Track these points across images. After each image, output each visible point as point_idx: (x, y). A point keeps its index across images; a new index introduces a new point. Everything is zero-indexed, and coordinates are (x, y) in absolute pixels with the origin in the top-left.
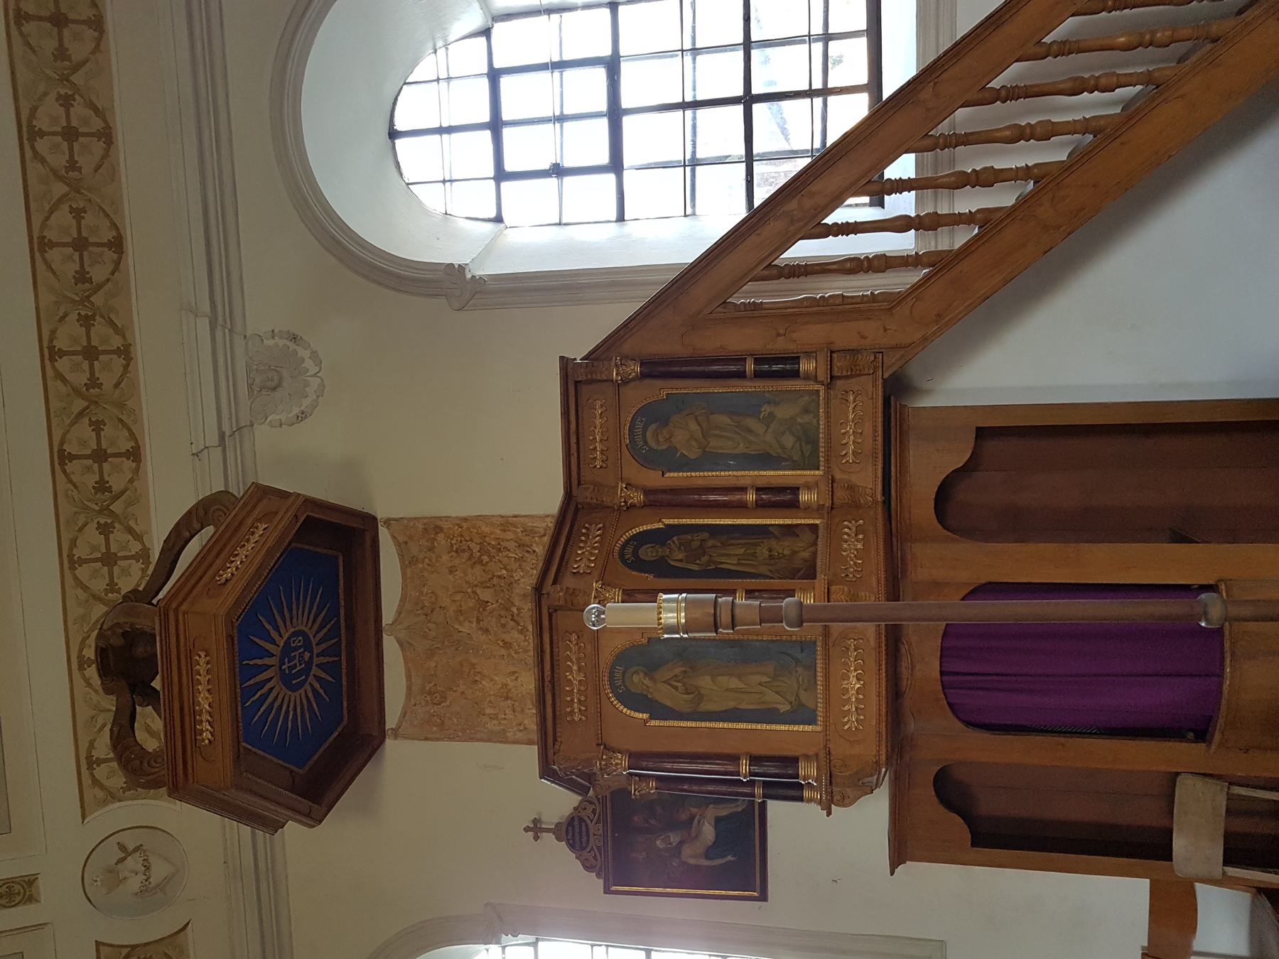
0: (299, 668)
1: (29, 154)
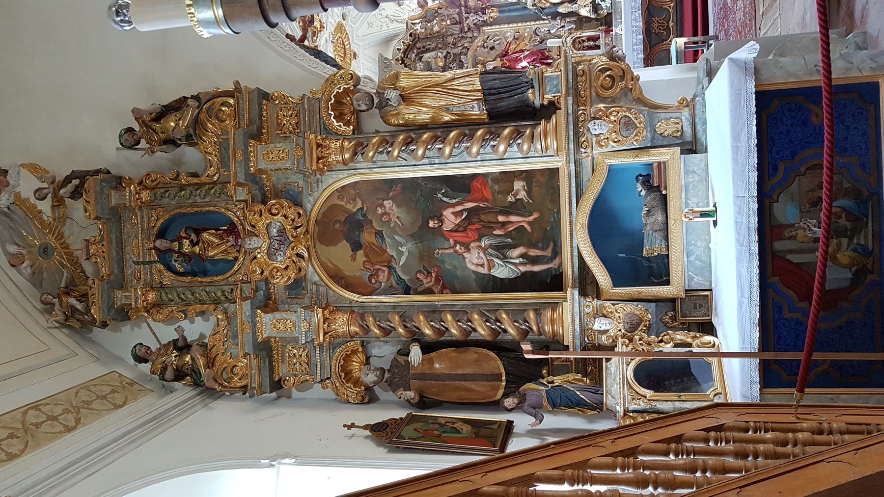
0: (343, 203)
1: (25, 408)
